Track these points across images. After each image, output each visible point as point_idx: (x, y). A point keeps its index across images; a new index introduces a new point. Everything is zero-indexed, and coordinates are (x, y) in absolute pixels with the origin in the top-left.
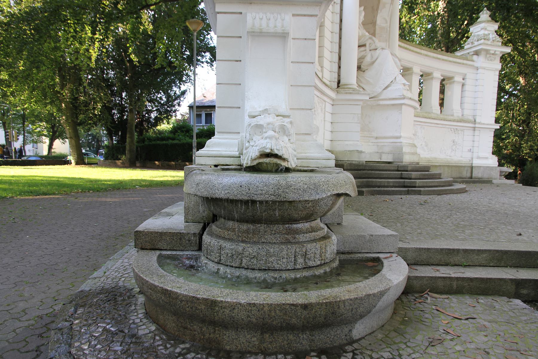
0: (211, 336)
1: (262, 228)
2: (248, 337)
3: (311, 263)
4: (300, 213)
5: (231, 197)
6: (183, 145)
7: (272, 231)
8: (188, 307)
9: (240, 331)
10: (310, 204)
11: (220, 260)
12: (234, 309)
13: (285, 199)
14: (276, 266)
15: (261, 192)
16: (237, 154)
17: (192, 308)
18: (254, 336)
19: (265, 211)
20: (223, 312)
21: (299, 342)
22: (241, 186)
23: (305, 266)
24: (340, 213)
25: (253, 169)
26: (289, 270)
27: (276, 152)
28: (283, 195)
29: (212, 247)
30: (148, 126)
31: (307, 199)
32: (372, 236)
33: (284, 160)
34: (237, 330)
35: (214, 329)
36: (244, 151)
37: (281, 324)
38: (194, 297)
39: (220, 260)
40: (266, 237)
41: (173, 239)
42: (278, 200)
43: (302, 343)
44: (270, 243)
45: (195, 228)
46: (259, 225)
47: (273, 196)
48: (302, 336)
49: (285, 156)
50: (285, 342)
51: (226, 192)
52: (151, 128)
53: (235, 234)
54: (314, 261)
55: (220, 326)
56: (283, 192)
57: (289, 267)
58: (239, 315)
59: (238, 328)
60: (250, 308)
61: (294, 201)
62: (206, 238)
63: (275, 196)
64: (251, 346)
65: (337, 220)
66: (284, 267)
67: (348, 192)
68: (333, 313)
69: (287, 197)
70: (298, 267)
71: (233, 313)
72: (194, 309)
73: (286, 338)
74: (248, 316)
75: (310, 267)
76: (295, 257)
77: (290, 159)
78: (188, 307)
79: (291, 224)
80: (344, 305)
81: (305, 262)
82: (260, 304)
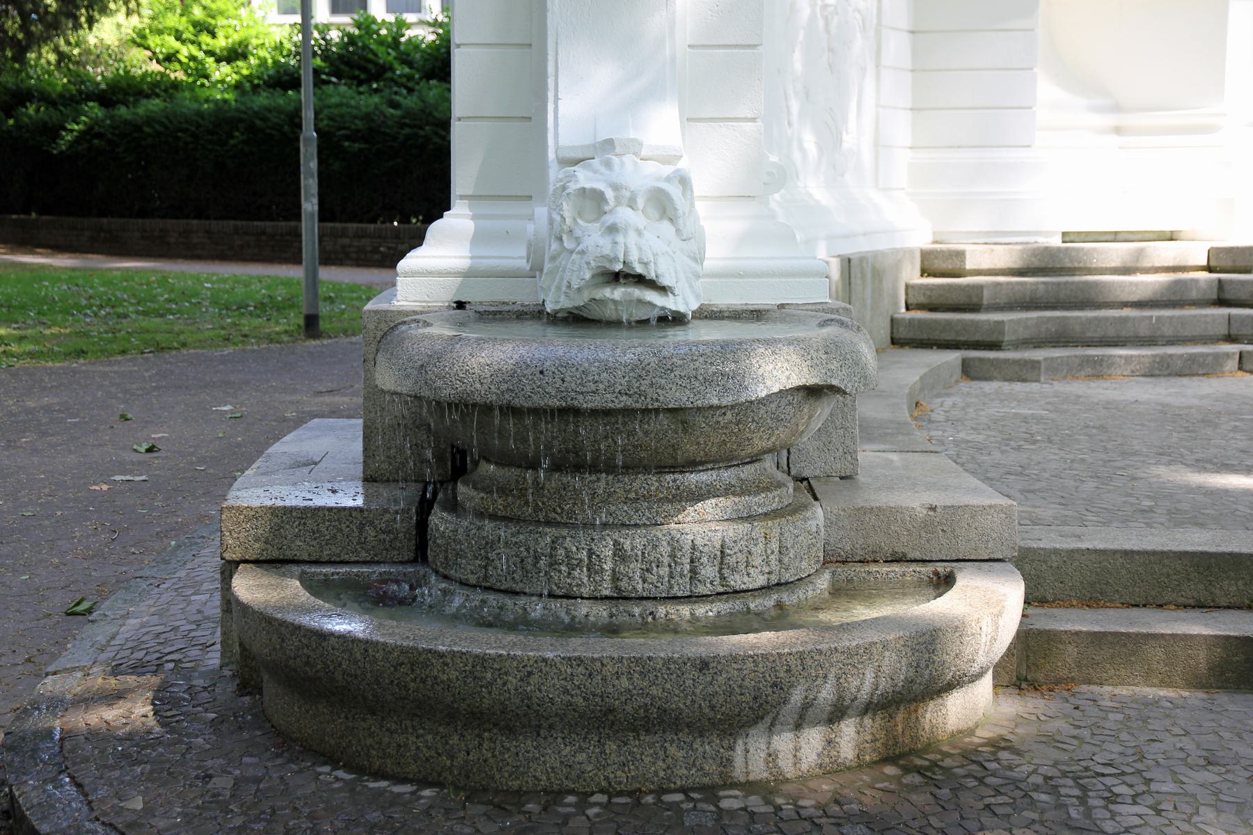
0: (471, 757)
1: (602, 484)
2: (564, 753)
3: (737, 581)
4: (701, 440)
5: (517, 402)
6: (333, 219)
7: (629, 491)
8: (414, 680)
9: (545, 738)
10: (729, 415)
11: (486, 577)
12: (530, 674)
13: (656, 405)
14: (640, 587)
15: (593, 387)
16: (523, 264)
17: (423, 681)
18: (581, 749)
19: (606, 437)
20: (505, 684)
21: (694, 765)
22: (542, 372)
23: (721, 589)
24: (848, 442)
25: (576, 320)
26: (675, 598)
27: (639, 269)
28: (651, 393)
29: (460, 542)
30: (24, 27)
31: (715, 401)
32: (933, 509)
33: (663, 290)
34: (538, 735)
35: (479, 736)
36: (547, 266)
37: (646, 711)
38: (430, 651)
39: (486, 577)
40: (613, 508)
41: (341, 530)
42: (638, 406)
43: (702, 769)
44: (623, 525)
45: (402, 497)
46: (594, 477)
47: (624, 398)
48: (701, 749)
49: (665, 281)
50: (660, 763)
51: (504, 387)
52: (46, 39)
53: (527, 503)
54: (748, 575)
55: (495, 725)
56: (652, 385)
57: (676, 591)
58: (544, 688)
59: (539, 726)
60: (569, 671)
61: (681, 409)
62: (439, 520)
63: (630, 396)
64: (574, 774)
65: (840, 467)
66: (663, 590)
67: (835, 382)
68: (775, 685)
69: (661, 398)
70: (701, 589)
71: (529, 684)
72: (429, 682)
73: (661, 753)
74: (566, 692)
75: (736, 592)
76: (692, 561)
77: (681, 287)
78: (414, 680)
79: (682, 472)
80: (802, 664)
81: (723, 578)
82: (593, 660)
